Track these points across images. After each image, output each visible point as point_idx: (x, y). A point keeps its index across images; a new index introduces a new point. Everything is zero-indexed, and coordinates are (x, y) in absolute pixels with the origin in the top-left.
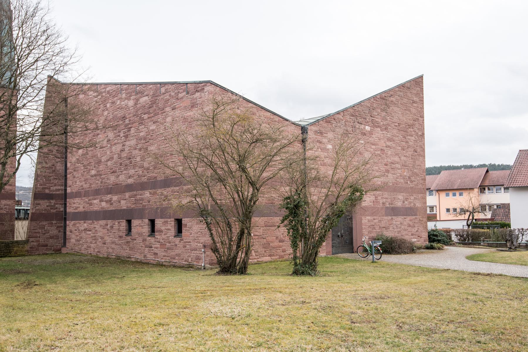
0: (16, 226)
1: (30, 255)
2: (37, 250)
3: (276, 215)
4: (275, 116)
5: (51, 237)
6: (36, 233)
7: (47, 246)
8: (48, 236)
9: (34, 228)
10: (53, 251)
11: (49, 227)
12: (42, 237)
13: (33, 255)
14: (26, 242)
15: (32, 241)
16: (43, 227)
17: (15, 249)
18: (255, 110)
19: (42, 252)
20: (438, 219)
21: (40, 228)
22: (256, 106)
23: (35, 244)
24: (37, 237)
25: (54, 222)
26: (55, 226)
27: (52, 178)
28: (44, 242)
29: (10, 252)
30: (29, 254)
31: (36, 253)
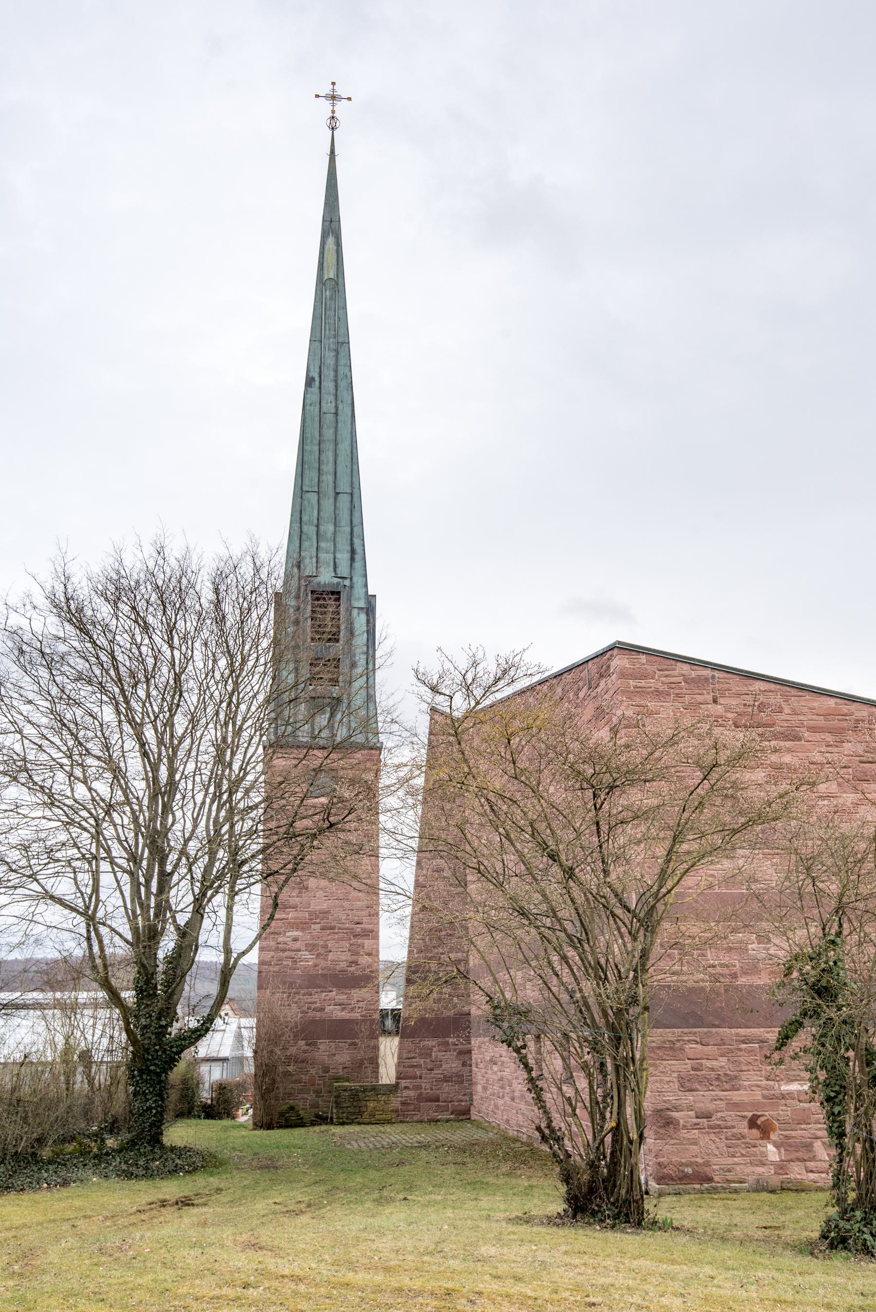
0: (382, 1047)
1: (401, 1122)
2: (417, 1109)
3: (767, 1023)
4: (854, 707)
5: (447, 1079)
6: (413, 1066)
7: (438, 1100)
8: (439, 1076)
9: (409, 1056)
10: (452, 1113)
11: (440, 1054)
12: (426, 1078)
13: (408, 1122)
14: (393, 1089)
15: (406, 1088)
16: (427, 1053)
17: (371, 1105)
18: (776, 699)
19: (428, 1115)
20: (309, 389)
21: (421, 1055)
22: (778, 687)
23: (412, 1093)
24: (415, 1078)
25: (451, 1040)
26: (455, 1050)
27: (444, 933)
28: (432, 1089)
29: (360, 1113)
30: (401, 1118)
31: (415, 1118)
